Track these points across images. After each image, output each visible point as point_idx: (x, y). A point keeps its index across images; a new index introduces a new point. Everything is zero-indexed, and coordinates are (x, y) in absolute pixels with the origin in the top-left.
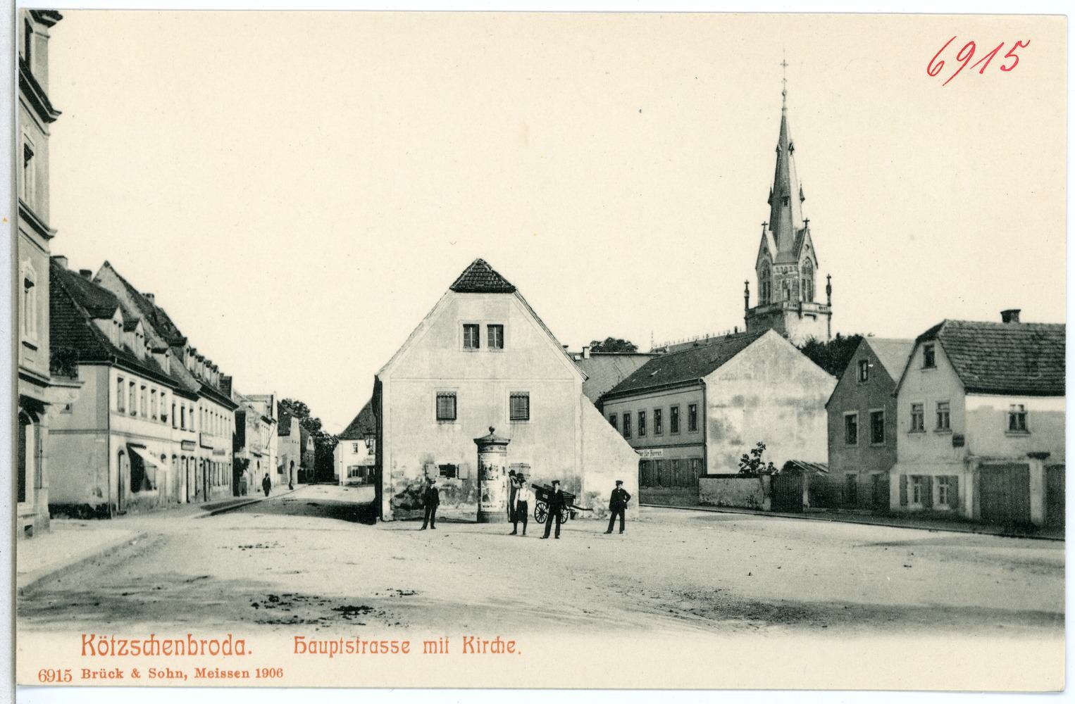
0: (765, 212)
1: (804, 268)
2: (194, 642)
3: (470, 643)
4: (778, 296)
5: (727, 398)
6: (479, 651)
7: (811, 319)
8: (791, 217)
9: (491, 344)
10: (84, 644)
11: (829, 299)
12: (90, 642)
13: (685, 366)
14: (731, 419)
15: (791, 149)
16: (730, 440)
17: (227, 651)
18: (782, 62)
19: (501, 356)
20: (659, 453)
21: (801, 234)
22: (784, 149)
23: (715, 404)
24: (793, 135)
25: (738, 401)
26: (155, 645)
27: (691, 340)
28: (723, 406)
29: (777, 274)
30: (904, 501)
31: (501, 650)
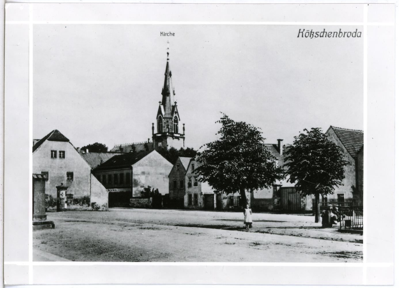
0: (160, 98)
1: (174, 120)
2: (342, 32)
3: (162, 33)
4: (165, 130)
5: (139, 172)
6: (164, 35)
7: (177, 140)
8: (170, 101)
9: (60, 157)
10: (299, 32)
11: (184, 133)
12: (302, 32)
13: (129, 156)
14: (141, 179)
15: (170, 75)
16: (140, 186)
17: (354, 35)
18: (167, 42)
19: (64, 160)
20: (116, 190)
21: (174, 107)
22: (168, 74)
23: (136, 174)
24: (171, 69)
25: (143, 173)
26: (325, 33)
27: (131, 144)
28: (139, 175)
29: (164, 122)
30: (235, 203)
31: (324, 36)
